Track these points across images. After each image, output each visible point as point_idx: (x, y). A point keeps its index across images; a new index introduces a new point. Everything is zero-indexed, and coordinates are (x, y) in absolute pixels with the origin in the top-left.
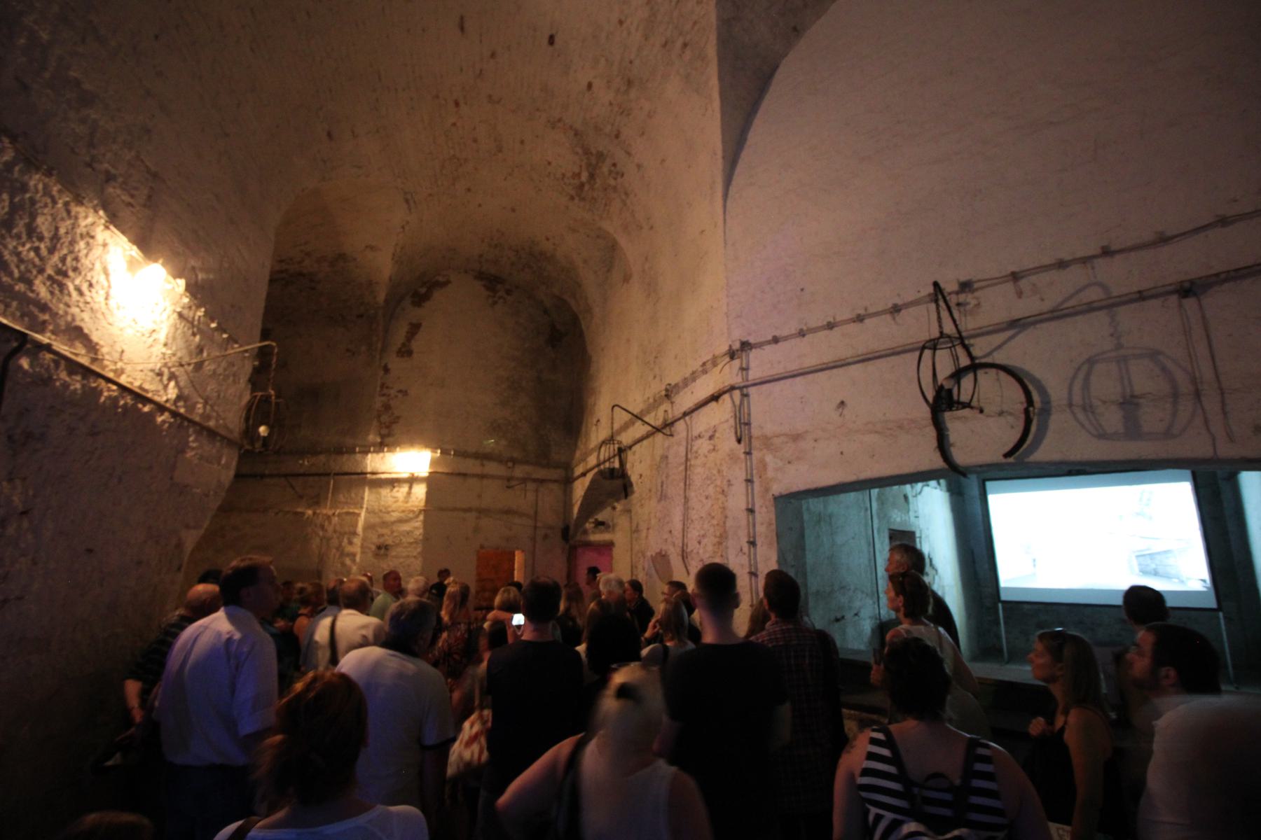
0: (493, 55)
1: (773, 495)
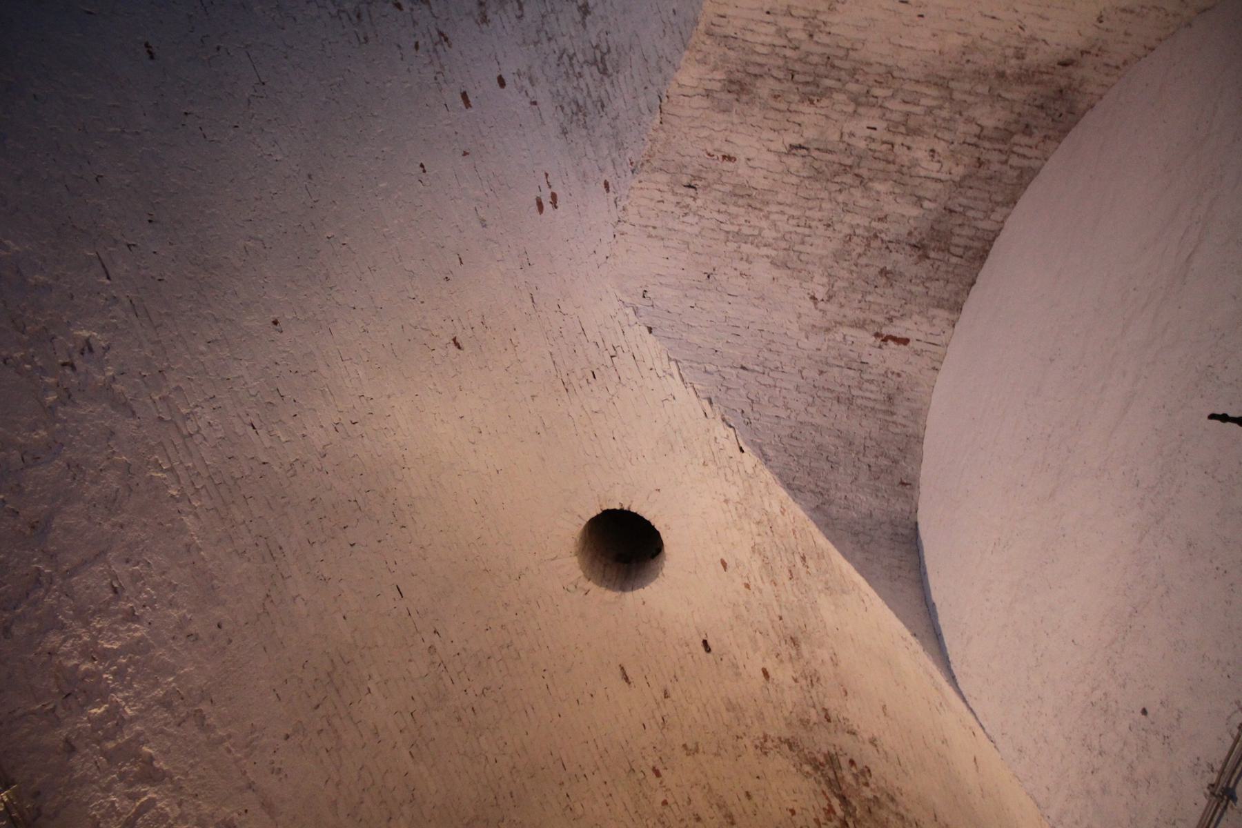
0: (666, 695)
1: (826, 230)
